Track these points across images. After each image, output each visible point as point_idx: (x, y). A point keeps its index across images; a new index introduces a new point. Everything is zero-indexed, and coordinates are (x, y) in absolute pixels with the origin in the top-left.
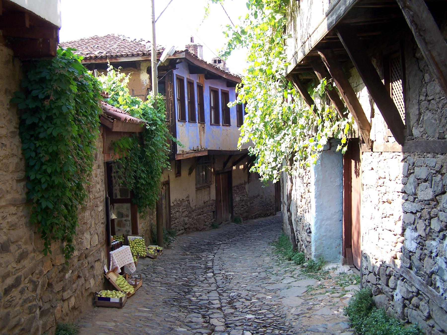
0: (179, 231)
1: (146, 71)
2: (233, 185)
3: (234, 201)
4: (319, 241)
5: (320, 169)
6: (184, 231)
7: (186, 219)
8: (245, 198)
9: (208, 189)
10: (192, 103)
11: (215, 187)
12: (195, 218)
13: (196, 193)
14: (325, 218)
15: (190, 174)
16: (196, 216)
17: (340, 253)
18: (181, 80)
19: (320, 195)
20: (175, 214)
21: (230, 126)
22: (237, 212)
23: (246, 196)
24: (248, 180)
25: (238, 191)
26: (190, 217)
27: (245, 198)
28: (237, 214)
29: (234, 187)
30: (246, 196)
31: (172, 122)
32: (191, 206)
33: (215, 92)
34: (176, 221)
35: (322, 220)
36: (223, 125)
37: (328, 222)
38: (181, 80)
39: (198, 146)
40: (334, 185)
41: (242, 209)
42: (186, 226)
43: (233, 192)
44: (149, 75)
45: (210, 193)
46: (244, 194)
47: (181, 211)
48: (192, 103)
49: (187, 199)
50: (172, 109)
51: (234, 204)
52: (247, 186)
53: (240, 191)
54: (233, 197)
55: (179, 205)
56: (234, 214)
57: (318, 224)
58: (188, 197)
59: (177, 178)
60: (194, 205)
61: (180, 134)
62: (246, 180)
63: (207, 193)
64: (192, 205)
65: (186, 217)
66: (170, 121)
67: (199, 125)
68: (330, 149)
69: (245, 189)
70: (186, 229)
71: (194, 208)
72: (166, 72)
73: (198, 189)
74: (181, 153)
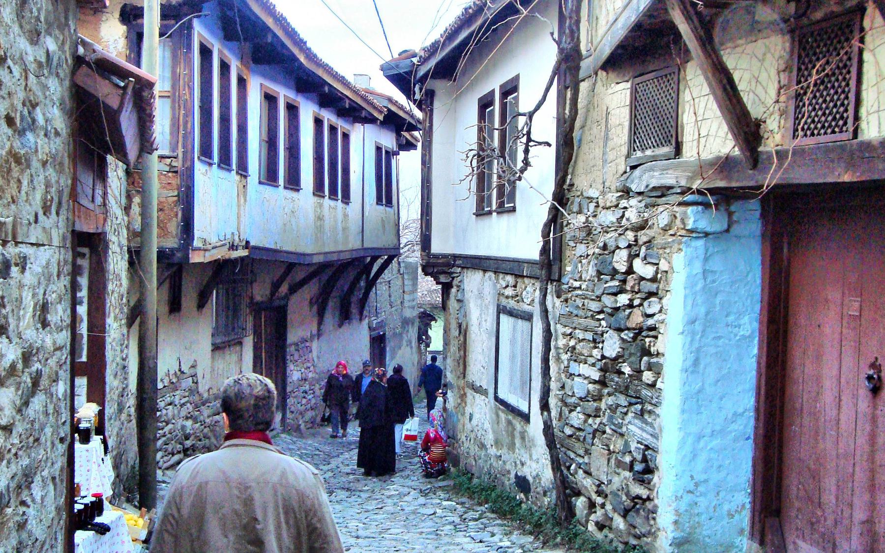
0: (173, 454)
1: (117, 15)
2: (289, 341)
3: (289, 380)
4: (688, 498)
5: (700, 286)
6: (181, 456)
7: (189, 423)
8: (311, 375)
9: (238, 348)
10: (225, 120)
11: (251, 341)
12: (208, 420)
13: (213, 358)
14: (708, 431)
15: (201, 305)
16: (209, 417)
17: (741, 532)
18: (206, 52)
19: (696, 362)
20: (164, 412)
21: (298, 190)
22: (293, 409)
23: (312, 368)
24: (319, 330)
25: (296, 356)
26: (195, 420)
27: (311, 375)
28: (292, 412)
29: (291, 345)
30: (312, 368)
31: (184, 161)
32: (201, 389)
33: (270, 99)
34: (167, 429)
35: (700, 437)
36: (285, 188)
37: (715, 443)
38: (206, 52)
39: (233, 233)
40: (736, 335)
41: (304, 401)
42: (188, 443)
43: (288, 357)
44: (125, 27)
45: (241, 360)
46: (309, 365)
47: (177, 402)
48: (225, 120)
49: (192, 371)
50: (186, 123)
51: (289, 389)
52: (315, 345)
53: (300, 356)
54: (288, 372)
55: (173, 387)
56: (289, 415)
57: (688, 448)
58: (193, 367)
59: (172, 316)
60: (207, 388)
61: (201, 195)
62: (315, 331)
63: (234, 357)
64: (203, 388)
65: (187, 418)
66: (180, 156)
67: (238, 178)
68: (727, 231)
69: (311, 351)
70: (187, 449)
71: (206, 395)
72: (173, 22)
73: (217, 348)
74: (200, 245)
